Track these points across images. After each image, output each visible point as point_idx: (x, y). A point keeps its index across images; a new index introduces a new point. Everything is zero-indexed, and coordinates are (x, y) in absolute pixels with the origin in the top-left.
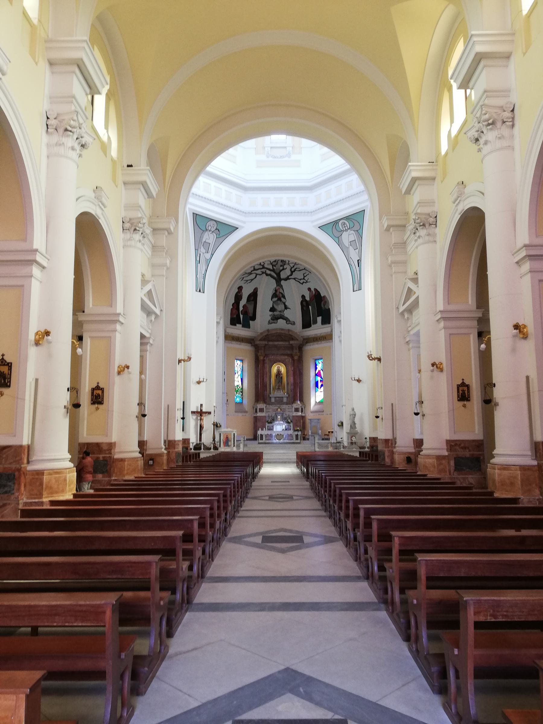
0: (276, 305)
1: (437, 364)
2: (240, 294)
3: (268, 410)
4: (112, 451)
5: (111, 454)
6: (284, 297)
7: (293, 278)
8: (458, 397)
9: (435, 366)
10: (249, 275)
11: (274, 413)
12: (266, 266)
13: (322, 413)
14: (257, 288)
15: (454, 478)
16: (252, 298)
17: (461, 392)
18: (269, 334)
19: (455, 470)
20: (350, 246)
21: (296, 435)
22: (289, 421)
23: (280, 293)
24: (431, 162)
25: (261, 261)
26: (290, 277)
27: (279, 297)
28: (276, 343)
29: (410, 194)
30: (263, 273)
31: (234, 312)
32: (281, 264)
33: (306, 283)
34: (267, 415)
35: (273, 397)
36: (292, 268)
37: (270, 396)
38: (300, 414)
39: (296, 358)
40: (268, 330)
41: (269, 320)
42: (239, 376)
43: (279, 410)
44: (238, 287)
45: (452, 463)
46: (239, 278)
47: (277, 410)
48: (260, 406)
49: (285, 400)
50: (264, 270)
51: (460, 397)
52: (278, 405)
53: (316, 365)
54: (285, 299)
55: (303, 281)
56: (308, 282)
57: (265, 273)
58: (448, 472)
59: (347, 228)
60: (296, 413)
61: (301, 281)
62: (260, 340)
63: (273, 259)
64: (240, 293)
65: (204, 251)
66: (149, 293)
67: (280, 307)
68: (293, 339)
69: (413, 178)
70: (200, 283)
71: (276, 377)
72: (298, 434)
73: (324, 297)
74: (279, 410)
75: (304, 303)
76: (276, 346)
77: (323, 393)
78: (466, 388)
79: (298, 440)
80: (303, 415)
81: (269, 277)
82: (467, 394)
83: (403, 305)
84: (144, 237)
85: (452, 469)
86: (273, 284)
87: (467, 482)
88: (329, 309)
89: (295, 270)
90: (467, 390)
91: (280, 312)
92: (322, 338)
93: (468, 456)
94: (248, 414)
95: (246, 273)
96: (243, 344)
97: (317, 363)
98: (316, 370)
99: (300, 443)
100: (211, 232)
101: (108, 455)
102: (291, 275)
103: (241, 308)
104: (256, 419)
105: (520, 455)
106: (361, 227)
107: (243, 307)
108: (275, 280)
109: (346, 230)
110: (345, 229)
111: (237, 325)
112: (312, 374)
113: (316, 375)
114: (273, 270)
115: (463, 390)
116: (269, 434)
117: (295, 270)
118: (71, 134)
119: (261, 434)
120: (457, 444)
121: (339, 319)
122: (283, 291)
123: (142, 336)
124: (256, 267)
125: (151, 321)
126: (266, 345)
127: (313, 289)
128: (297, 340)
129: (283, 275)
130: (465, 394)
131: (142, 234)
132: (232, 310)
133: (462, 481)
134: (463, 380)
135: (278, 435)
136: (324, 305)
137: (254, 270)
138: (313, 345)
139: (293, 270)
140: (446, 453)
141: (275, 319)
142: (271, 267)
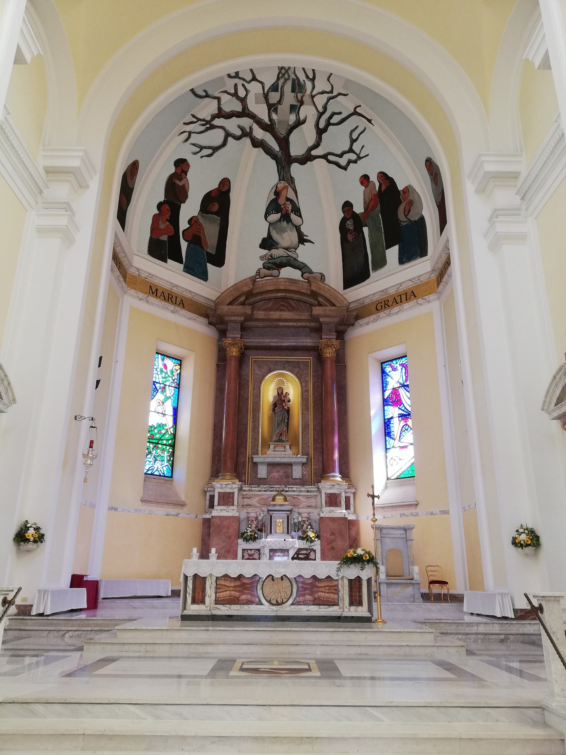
0: (277, 233)
2: (181, 184)
3: (247, 501)
6: (297, 211)
10: (207, 130)
11: (265, 509)
13: (413, 510)
14: (188, 166)
16: (215, 207)
21: (350, 581)
22: (312, 535)
23: (288, 199)
26: (314, 153)
27: (284, 212)
31: (162, 226)
33: (355, 162)
34: (243, 515)
35: (263, 463)
37: (255, 460)
38: (340, 512)
39: (329, 353)
41: (259, 269)
42: (167, 398)
43: (280, 500)
47: (274, 500)
49: (297, 472)
50: (246, 122)
54: (300, 216)
61: (343, 161)
64: (181, 180)
71: (274, 410)
72: (359, 579)
74: (280, 500)
75: (350, 224)
77: (411, 449)
79: (360, 604)
80: (351, 517)
81: (259, 151)
91: (287, 249)
92: (404, 297)
94: (185, 509)
95: (199, 120)
96: (183, 312)
97: (388, 369)
98: (384, 391)
99: (367, 620)
102: (316, 146)
103: (183, 225)
104: (207, 523)
107: (190, 222)
108: (273, 163)
111: (169, 261)
112: (376, 399)
113: (385, 402)
114: (269, 128)
116: (248, 574)
117: (328, 124)
119: (196, 576)
127: (374, 178)
132: (155, 218)
135: (269, 582)
136: (407, 212)
137: (221, 114)
138: (375, 320)
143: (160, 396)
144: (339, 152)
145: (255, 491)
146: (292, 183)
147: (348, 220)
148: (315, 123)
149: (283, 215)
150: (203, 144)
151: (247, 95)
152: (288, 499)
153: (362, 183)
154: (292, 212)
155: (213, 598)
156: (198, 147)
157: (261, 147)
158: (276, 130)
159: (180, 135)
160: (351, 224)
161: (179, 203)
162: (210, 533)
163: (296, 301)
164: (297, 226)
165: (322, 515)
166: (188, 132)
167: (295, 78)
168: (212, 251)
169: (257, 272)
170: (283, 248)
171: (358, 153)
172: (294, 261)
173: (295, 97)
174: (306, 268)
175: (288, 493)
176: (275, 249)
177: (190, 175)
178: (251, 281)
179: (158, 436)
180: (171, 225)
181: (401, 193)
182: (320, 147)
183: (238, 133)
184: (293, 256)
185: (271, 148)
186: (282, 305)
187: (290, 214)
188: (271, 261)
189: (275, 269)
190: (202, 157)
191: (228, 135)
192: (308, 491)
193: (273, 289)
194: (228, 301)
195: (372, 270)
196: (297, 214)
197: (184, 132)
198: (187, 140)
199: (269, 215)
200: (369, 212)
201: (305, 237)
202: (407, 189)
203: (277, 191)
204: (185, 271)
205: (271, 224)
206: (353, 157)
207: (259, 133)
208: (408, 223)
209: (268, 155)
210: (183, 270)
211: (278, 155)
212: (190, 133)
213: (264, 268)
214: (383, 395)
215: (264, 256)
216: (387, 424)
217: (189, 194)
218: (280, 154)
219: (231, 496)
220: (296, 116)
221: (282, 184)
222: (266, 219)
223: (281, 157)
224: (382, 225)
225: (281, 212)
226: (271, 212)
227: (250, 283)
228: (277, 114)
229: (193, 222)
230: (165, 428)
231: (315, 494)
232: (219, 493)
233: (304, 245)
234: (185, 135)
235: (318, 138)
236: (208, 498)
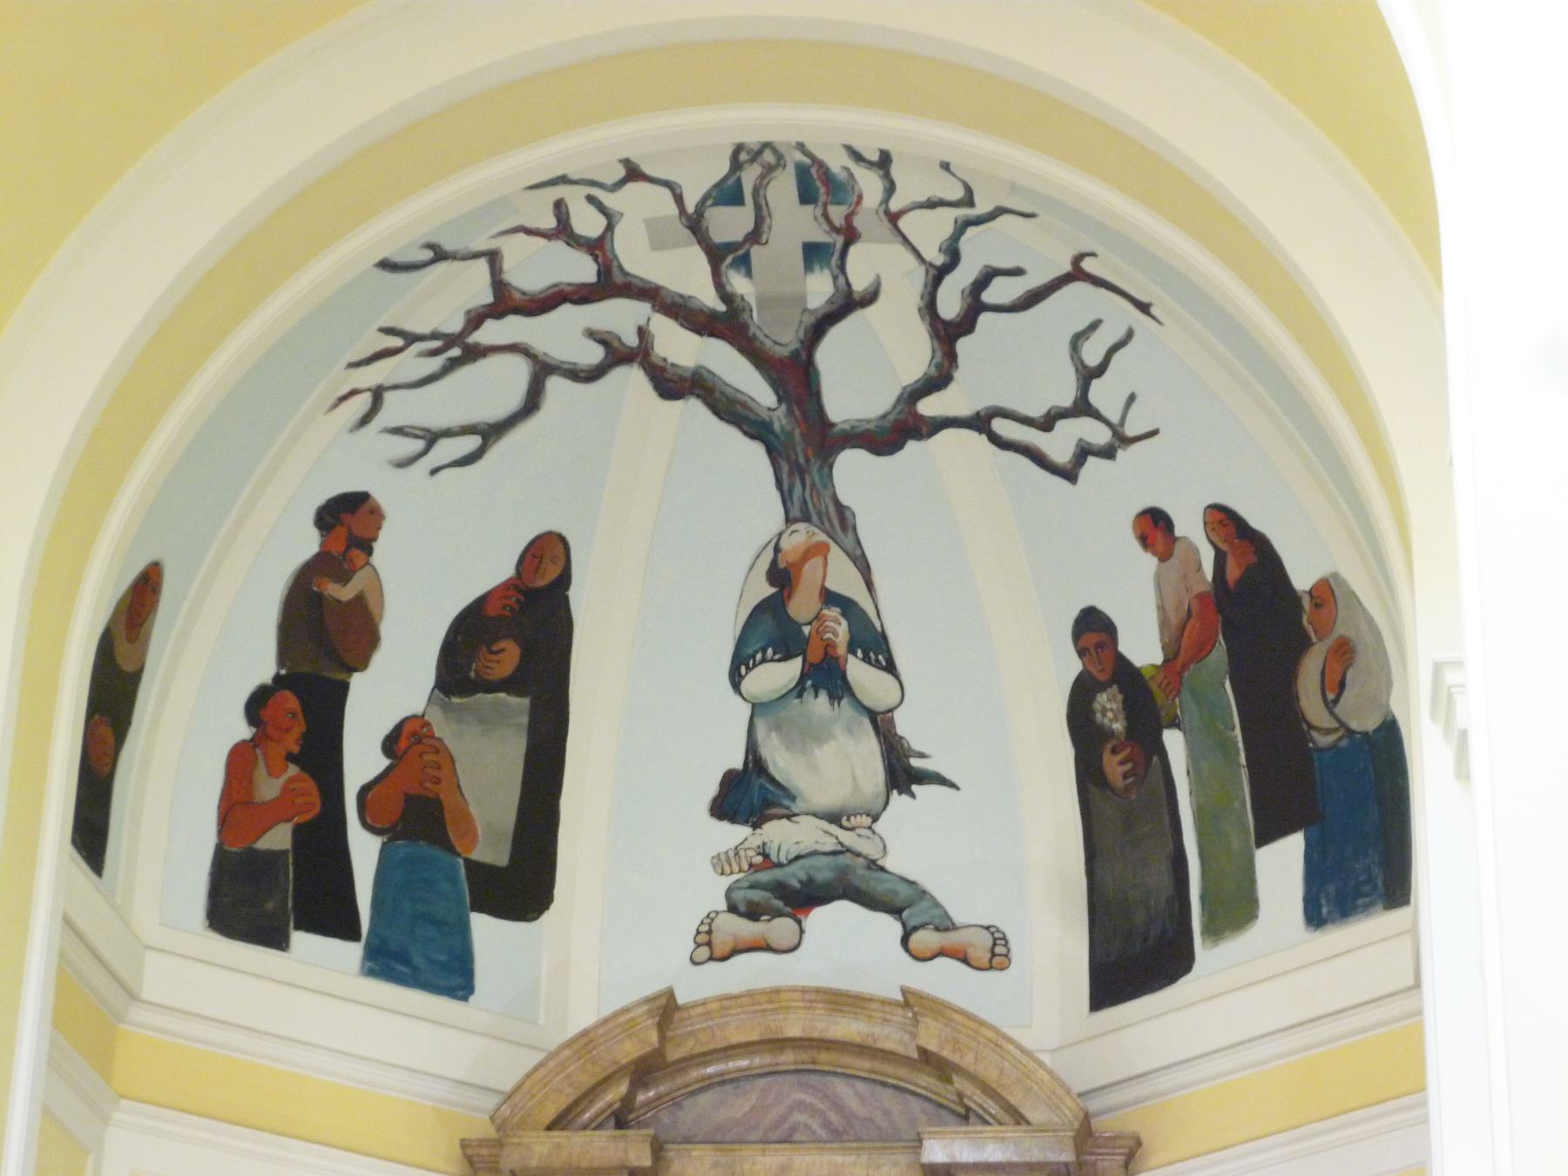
0: (789, 744)
2: (345, 593)
7: (964, 410)
10: (453, 365)
14: (377, 515)
16: (507, 658)
18: (673, 1054)
23: (830, 598)
26: (929, 407)
27: (815, 655)
30: (617, 355)
31: (268, 788)
33: (1108, 453)
40: (666, 1009)
41: (710, 918)
44: (321, 498)
54: (890, 668)
56: (1128, 441)
57: (639, 354)
61: (1059, 444)
64: (344, 578)
75: (1109, 708)
81: (693, 408)
89: (975, 307)
91: (834, 818)
95: (411, 338)
102: (937, 381)
107: (390, 744)
108: (757, 451)
111: (299, 939)
117: (975, 307)
127: (1190, 526)
132: (240, 762)
136: (1334, 687)
137: (505, 302)
139: (950, 305)
144: (1037, 411)
146: (844, 527)
147: (1103, 687)
148: (918, 298)
149: (812, 665)
150: (438, 422)
151: (610, 228)
153: (1145, 541)
154: (851, 649)
156: (417, 437)
157: (698, 396)
158: (752, 330)
159: (335, 406)
160: (1114, 706)
161: (341, 676)
163: (860, 1086)
164: (879, 713)
166: (369, 390)
167: (807, 161)
168: (493, 850)
169: (698, 933)
170: (815, 815)
171: (1115, 418)
172: (867, 873)
173: (821, 220)
174: (924, 904)
176: (780, 817)
177: (385, 553)
178: (650, 1013)
180: (306, 776)
181: (1306, 603)
182: (952, 387)
183: (593, 354)
184: (865, 852)
185: (739, 396)
186: (800, 1105)
187: (842, 661)
188: (764, 877)
189: (781, 914)
190: (434, 472)
191: (543, 370)
193: (755, 1037)
194: (551, 1112)
195: (1203, 933)
196: (877, 660)
197: (354, 393)
198: (365, 420)
199: (749, 669)
200: (1185, 667)
201: (915, 762)
202: (1326, 592)
203: (782, 565)
204: (370, 972)
205: (757, 708)
206: (1099, 435)
208: (1340, 739)
209: (728, 421)
210: (363, 967)
211: (771, 423)
212: (378, 394)
213: (732, 909)
215: (731, 854)
218: (780, 419)
220: (835, 278)
221: (800, 537)
223: (788, 428)
224: (1238, 732)
225: (804, 653)
226: (759, 656)
227: (649, 1022)
228: (749, 274)
229: (403, 743)
233: (913, 795)
234: (362, 403)
235: (939, 354)
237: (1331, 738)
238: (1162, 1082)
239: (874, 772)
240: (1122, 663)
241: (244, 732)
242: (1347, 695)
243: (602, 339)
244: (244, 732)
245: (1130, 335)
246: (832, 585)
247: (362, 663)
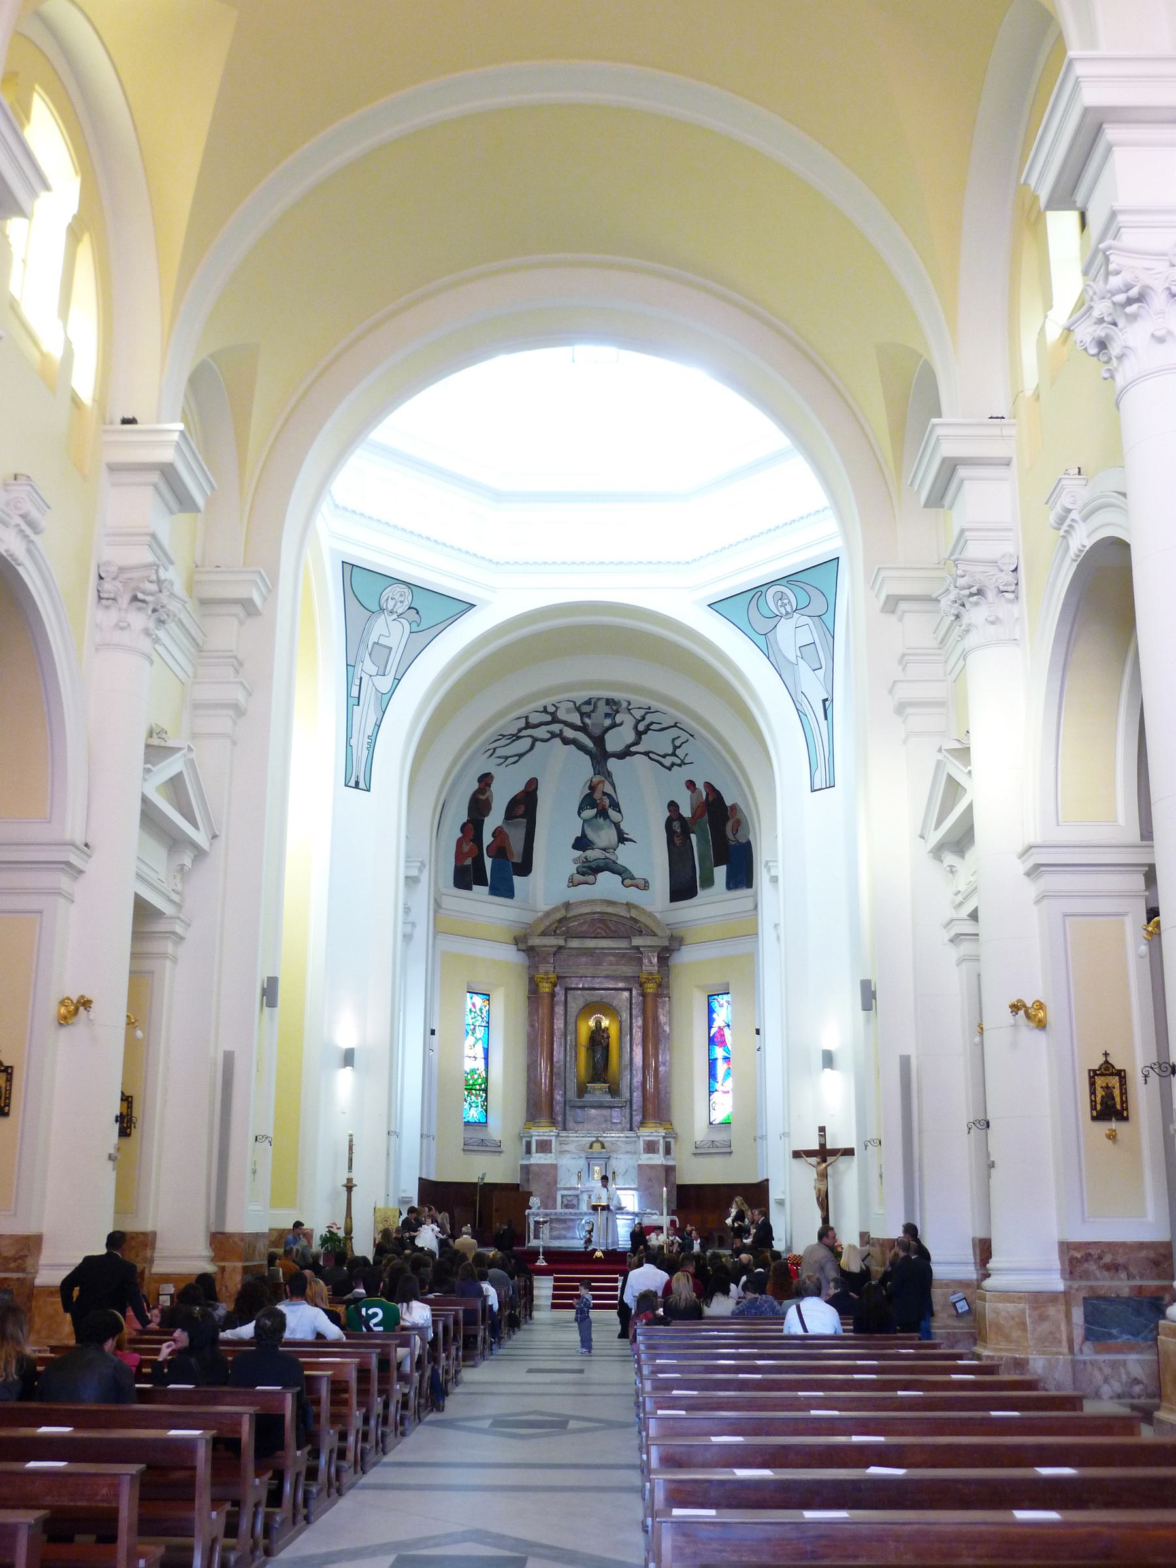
1: (1029, 1005)
2: (483, 797)
4: (29, 1261)
5: (23, 1270)
8: (1093, 1108)
9: (1022, 1012)
12: (561, 715)
14: (492, 777)
15: (1085, 1362)
16: (521, 809)
17: (1100, 1093)
18: (568, 916)
19: (1087, 1338)
20: (799, 659)
23: (604, 794)
24: (997, 418)
25: (547, 701)
26: (633, 749)
27: (600, 808)
28: (591, 943)
29: (943, 506)
30: (553, 735)
31: (466, 848)
32: (607, 710)
33: (680, 765)
36: (638, 722)
39: (651, 988)
40: (567, 906)
41: (572, 875)
42: (477, 1040)
45: (1078, 1315)
46: (482, 751)
47: (591, 1147)
48: (542, 1132)
50: (556, 728)
51: (1099, 1107)
52: (595, 1133)
53: (711, 1011)
54: (620, 812)
55: (671, 760)
58: (1065, 1343)
59: (789, 610)
60: (650, 1155)
61: (667, 761)
62: (544, 934)
63: (581, 696)
64: (483, 794)
65: (373, 669)
66: (175, 786)
67: (604, 836)
68: (640, 933)
69: (944, 460)
70: (359, 760)
73: (734, 807)
75: (676, 825)
76: (589, 952)
78: (1114, 1081)
81: (572, 747)
82: (1118, 1100)
83: (936, 828)
84: (161, 622)
85: (1079, 1333)
86: (583, 767)
87: (1124, 1376)
88: (749, 843)
89: (647, 729)
90: (1118, 1085)
91: (604, 850)
93: (1125, 1292)
95: (504, 736)
97: (715, 1005)
98: (710, 1027)
100: (395, 616)
101: (15, 1275)
102: (637, 743)
103: (487, 839)
105: (1039, 1270)
106: (831, 606)
107: (494, 835)
108: (588, 758)
109: (787, 613)
110: (784, 612)
111: (475, 887)
113: (711, 1041)
114: (583, 729)
115: (1107, 1087)
117: (647, 729)
118: (144, 605)
120: (1090, 1255)
121: (773, 873)
122: (615, 791)
123: (143, 912)
124: (535, 719)
125: (182, 866)
126: (560, 948)
127: (700, 785)
128: (655, 935)
129: (613, 742)
130: (1113, 1099)
131: (154, 611)
132: (459, 843)
133: (1107, 1371)
134: (1106, 1054)
136: (735, 831)
137: (528, 726)
139: (641, 727)
140: (1057, 1284)
141: (590, 870)
142: (576, 719)
143: (470, 1040)
145: (572, 1137)
152: (606, 1145)
153: (688, 787)
155: (548, 1235)
162: (528, 1179)
165: (640, 1162)
168: (517, 859)
175: (606, 1139)
179: (471, 1082)
183: (549, 735)
188: (586, 864)
191: (535, 740)
192: (627, 1137)
198: (491, 755)
201: (625, 836)
205: (585, 821)
206: (678, 762)
207: (569, 733)
212: (494, 749)
213: (578, 873)
214: (709, 1033)
216: (712, 1064)
217: (493, 806)
219: (546, 1145)
221: (597, 779)
222: (579, 815)
230: (478, 1072)
231: (635, 1139)
232: (537, 1140)
236: (524, 1143)
237: (733, 843)
238: (689, 924)
239: (614, 837)
240: (681, 816)
241: (460, 835)
242: (739, 833)
243: (551, 732)
244: (460, 835)
245: (687, 741)
246: (605, 790)
247: (487, 815)
